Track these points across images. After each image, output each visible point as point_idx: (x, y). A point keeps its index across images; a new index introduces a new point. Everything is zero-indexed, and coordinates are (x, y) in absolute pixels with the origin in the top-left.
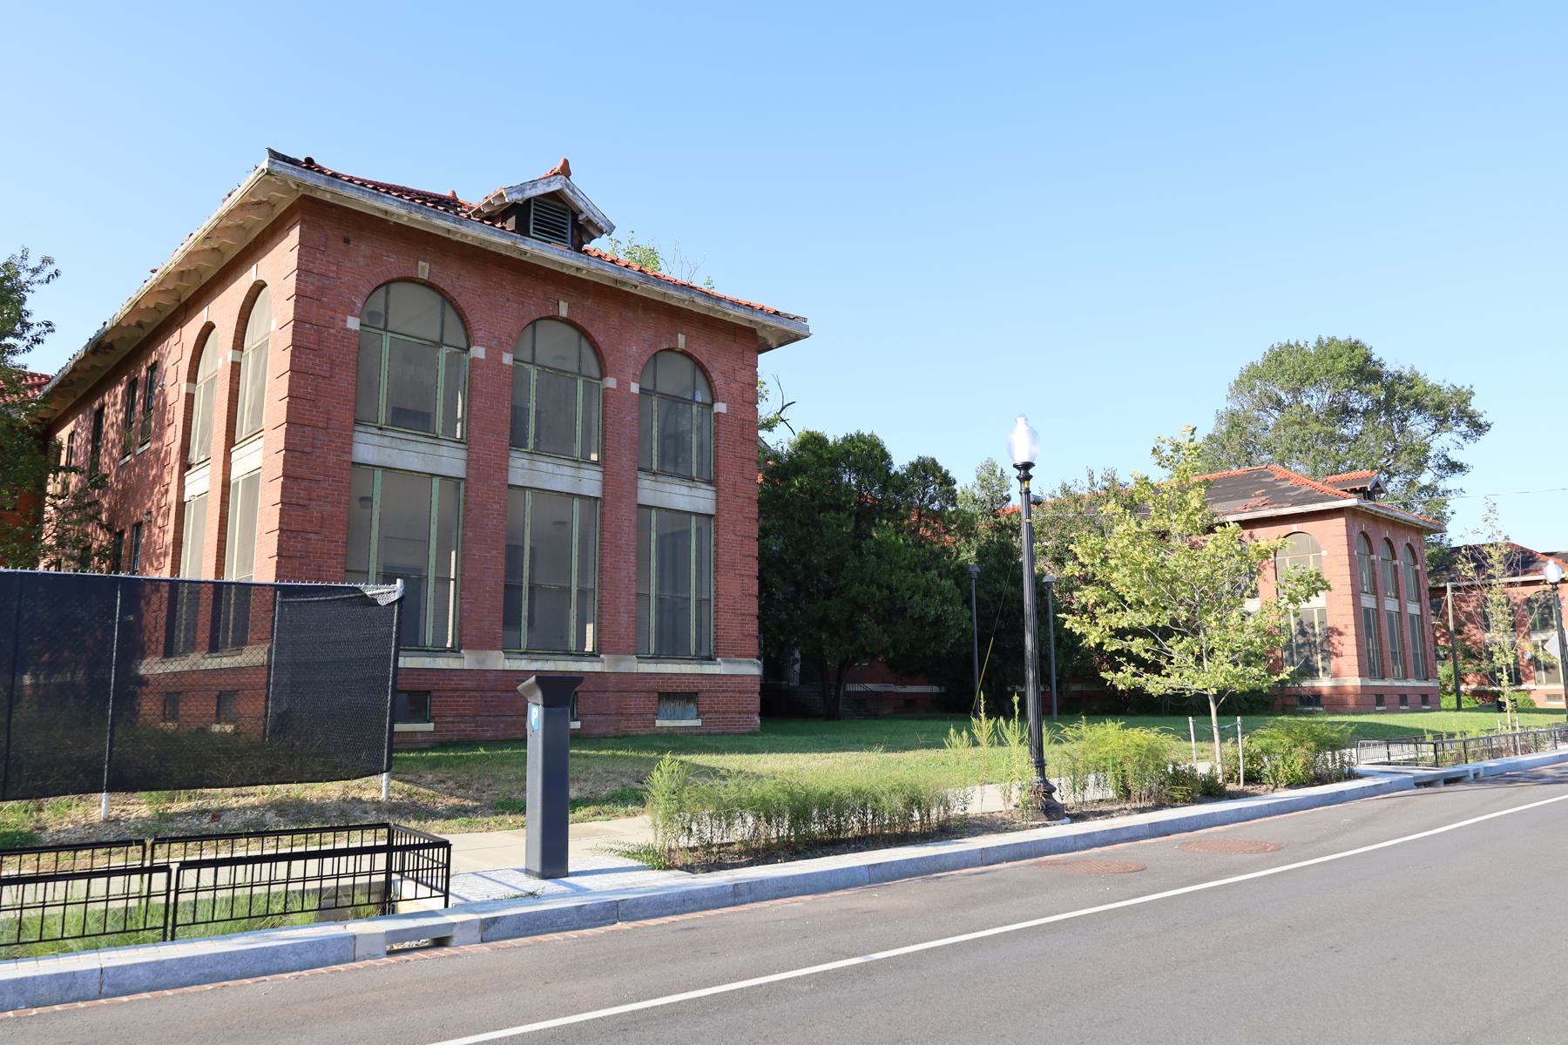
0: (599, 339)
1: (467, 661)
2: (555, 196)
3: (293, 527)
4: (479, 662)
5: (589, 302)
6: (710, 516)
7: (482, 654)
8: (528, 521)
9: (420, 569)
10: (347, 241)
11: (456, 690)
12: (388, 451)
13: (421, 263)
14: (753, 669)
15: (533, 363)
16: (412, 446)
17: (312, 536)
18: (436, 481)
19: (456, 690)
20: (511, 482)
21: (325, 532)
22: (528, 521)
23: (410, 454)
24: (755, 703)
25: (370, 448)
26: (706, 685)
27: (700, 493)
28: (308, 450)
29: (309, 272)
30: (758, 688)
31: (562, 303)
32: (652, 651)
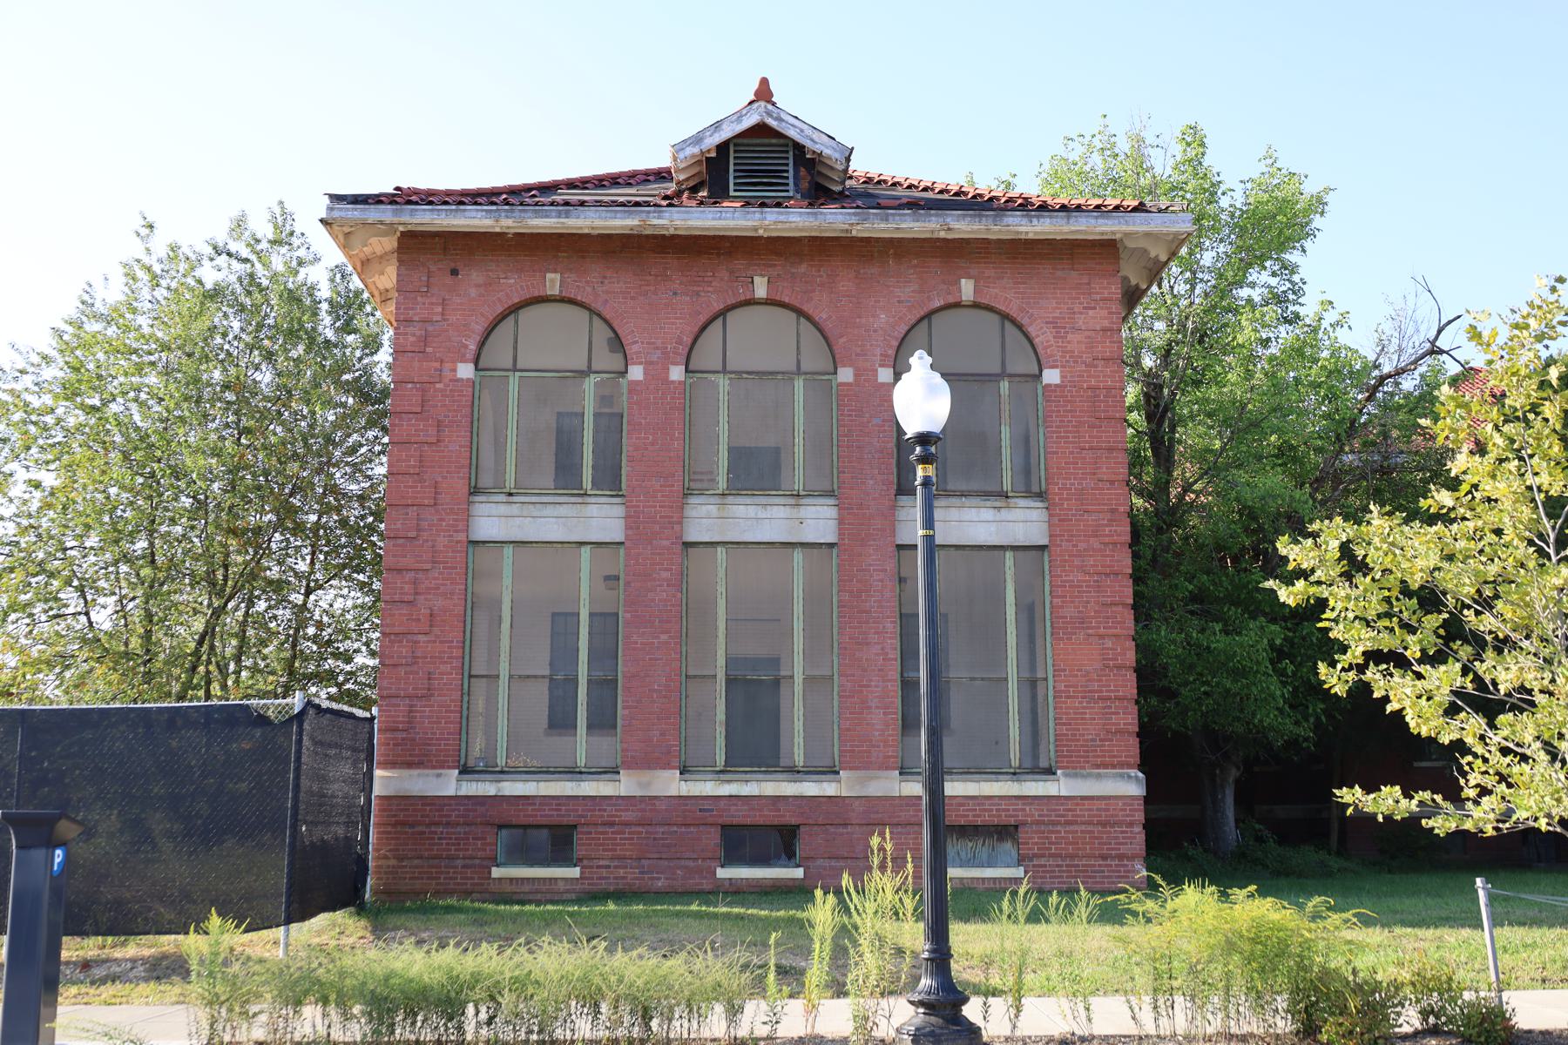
0: (821, 315)
1: (625, 785)
2: (761, 130)
3: (397, 629)
4: (641, 785)
5: (803, 268)
6: (1042, 548)
7: (646, 776)
8: (721, 589)
9: (775, 662)
10: (454, 272)
11: (612, 824)
12: (518, 521)
13: (549, 276)
14: (1131, 786)
15: (724, 371)
16: (549, 510)
17: (421, 638)
18: (586, 552)
19: (612, 824)
20: (692, 536)
21: (436, 630)
22: (721, 589)
23: (762, 520)
24: (1137, 839)
25: (705, 520)
26: (1033, 812)
27: (1017, 514)
28: (413, 534)
29: (409, 321)
30: (1140, 816)
31: (757, 279)
32: (1015, 762)
